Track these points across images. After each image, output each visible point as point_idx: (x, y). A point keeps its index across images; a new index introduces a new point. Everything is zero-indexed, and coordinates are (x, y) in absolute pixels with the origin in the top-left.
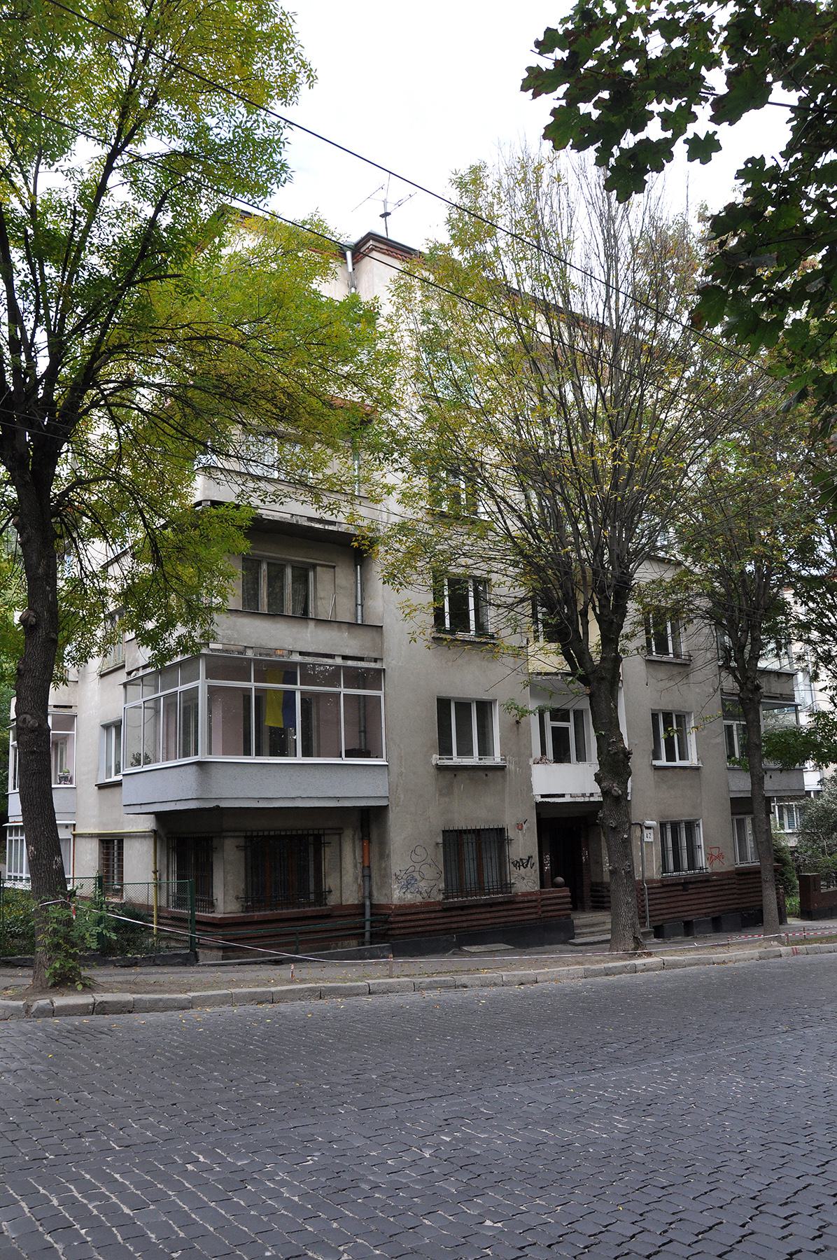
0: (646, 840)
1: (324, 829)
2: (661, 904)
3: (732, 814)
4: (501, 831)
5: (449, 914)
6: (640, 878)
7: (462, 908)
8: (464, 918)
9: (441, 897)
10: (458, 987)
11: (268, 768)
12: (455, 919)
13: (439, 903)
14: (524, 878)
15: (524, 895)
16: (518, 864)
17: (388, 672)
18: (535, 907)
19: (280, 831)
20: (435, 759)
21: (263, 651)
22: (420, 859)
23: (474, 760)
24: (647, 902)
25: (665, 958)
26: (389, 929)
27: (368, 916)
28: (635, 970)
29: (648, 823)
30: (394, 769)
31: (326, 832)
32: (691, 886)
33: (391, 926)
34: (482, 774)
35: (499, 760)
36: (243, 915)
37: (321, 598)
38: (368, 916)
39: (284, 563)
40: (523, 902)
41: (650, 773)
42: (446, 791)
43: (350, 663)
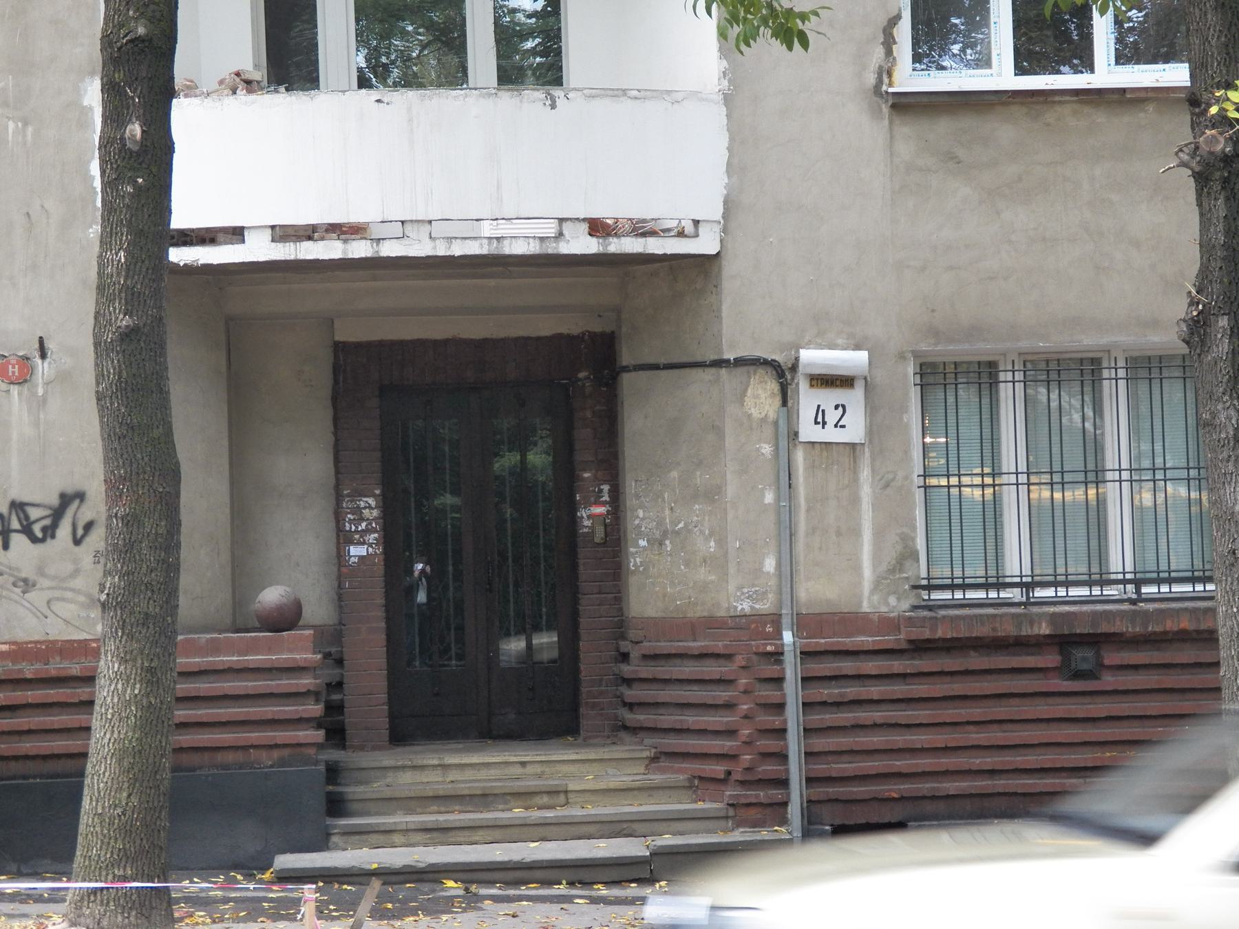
0: (809, 431)
6: (765, 606)
14: (27, 585)
29: (814, 357)
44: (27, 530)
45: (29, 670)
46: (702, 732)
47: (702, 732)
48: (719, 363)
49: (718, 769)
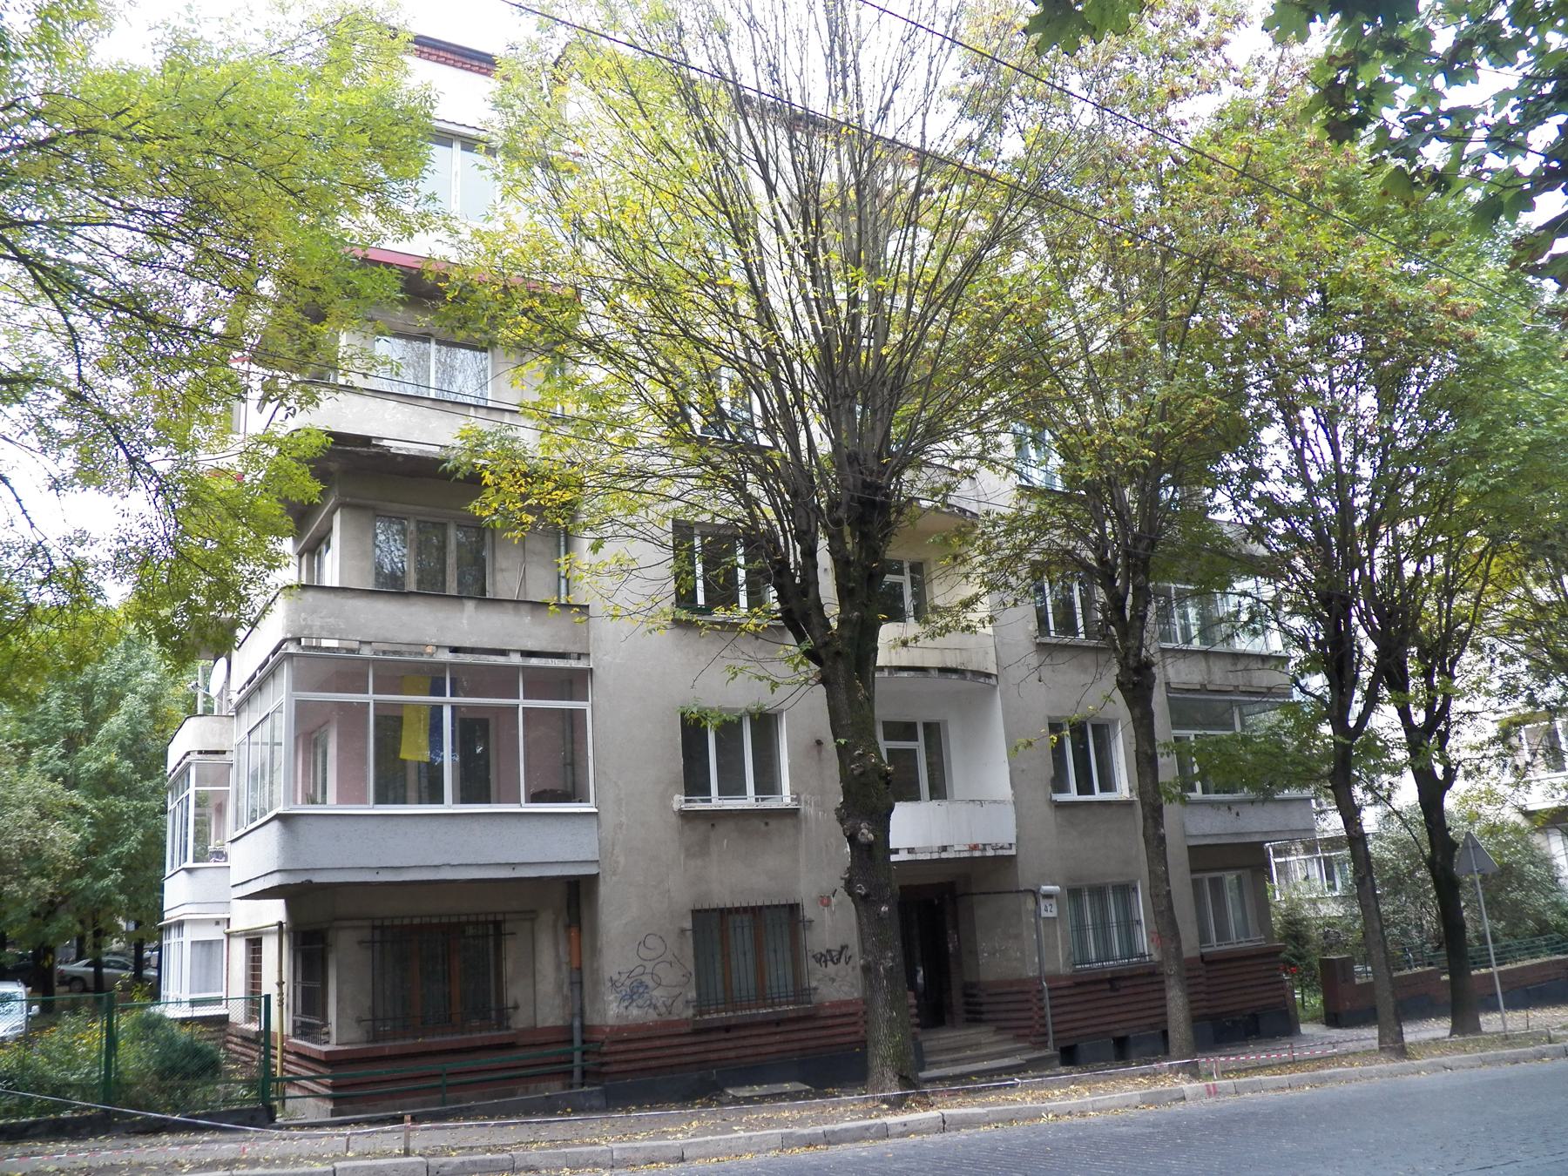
0: (1044, 914)
1: (504, 913)
2: (1074, 1012)
3: (1193, 871)
4: (794, 909)
5: (704, 1038)
6: (1036, 974)
7: (728, 1029)
8: (730, 1044)
9: (690, 1012)
10: (519, 1170)
11: (391, 823)
12: (715, 1046)
13: (686, 1021)
14: (833, 980)
15: (833, 1005)
16: (823, 958)
17: (597, 672)
18: (855, 1023)
19: (431, 916)
20: (679, 801)
21: (386, 647)
22: (653, 954)
23: (749, 801)
24: (1048, 1010)
25: (946, 1112)
26: (603, 1064)
27: (577, 1043)
28: (885, 1133)
29: (1046, 888)
30: (608, 818)
31: (507, 917)
32: (1123, 984)
33: (606, 1059)
34: (758, 824)
35: (787, 800)
36: (370, 1046)
37: (502, 570)
38: (577, 1043)
39: (444, 521)
40: (834, 1017)
41: (1047, 812)
42: (699, 850)
43: (534, 662)
44: (832, 960)
45: (837, 1012)
46: (1017, 1019)
47: (1017, 1019)
48: (1018, 892)
49: (1027, 1031)
